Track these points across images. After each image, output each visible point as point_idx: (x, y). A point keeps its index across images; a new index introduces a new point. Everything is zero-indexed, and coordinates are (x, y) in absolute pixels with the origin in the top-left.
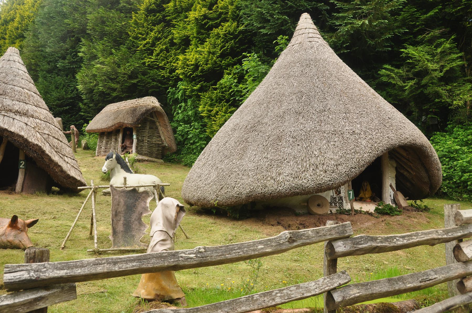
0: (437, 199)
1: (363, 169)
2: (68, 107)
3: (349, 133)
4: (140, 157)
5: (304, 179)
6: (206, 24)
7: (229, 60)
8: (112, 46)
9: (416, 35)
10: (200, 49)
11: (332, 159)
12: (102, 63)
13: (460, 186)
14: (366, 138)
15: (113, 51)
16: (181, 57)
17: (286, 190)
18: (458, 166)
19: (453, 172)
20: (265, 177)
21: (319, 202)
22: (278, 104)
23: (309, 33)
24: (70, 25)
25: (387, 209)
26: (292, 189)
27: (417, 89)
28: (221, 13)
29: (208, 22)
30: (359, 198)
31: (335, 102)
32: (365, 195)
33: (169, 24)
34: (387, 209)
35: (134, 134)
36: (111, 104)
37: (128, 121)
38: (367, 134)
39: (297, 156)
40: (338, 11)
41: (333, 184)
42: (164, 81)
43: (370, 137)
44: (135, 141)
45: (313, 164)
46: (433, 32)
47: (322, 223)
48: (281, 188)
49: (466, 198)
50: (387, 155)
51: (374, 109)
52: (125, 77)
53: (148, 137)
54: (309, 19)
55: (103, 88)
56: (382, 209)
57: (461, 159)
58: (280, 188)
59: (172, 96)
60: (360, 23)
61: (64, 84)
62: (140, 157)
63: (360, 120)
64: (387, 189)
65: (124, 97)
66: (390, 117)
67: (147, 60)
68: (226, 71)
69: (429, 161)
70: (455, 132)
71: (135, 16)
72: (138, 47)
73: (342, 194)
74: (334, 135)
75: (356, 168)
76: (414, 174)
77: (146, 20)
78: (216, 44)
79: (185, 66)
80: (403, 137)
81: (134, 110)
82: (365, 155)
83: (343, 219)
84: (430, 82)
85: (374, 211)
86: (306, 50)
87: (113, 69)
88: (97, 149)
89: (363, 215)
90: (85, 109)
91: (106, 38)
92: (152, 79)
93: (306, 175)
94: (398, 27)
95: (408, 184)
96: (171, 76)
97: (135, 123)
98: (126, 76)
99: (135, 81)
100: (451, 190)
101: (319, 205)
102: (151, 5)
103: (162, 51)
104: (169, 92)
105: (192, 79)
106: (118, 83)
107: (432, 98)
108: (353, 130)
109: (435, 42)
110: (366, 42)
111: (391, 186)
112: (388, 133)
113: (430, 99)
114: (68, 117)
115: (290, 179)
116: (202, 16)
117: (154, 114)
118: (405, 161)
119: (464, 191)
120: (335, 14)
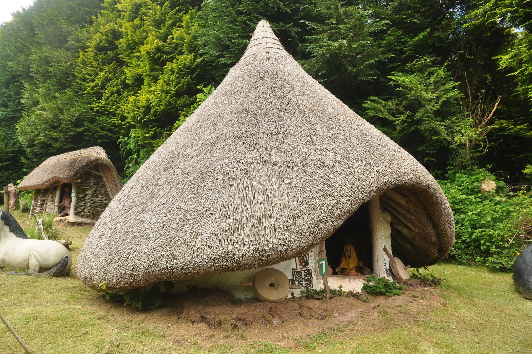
0: (443, 264)
1: (340, 223)
2: (8, 163)
3: (315, 164)
4: (80, 220)
5: (238, 242)
6: (159, 58)
7: (184, 99)
8: (56, 90)
9: (405, 62)
10: (153, 88)
11: (285, 207)
12: (44, 110)
13: (470, 246)
14: (343, 172)
15: (57, 94)
16: (131, 99)
17: (207, 263)
18: (466, 220)
19: (460, 229)
20: (173, 241)
21: (272, 280)
22: (211, 128)
23: (266, 43)
24: (12, 67)
25: (381, 286)
26: (216, 261)
27: (410, 125)
28: (177, 45)
29: (162, 56)
30: (340, 270)
31: (295, 122)
32: (348, 264)
33: (122, 63)
34: (381, 286)
35: (72, 191)
36: (52, 157)
37: (64, 175)
38: (344, 166)
39: (227, 203)
40: (311, 32)
41: (287, 249)
42: (116, 130)
43: (349, 170)
44: (74, 200)
45: (253, 217)
46: (423, 58)
47: (275, 315)
48: (197, 260)
49: (479, 261)
50: (378, 201)
51: (355, 132)
52: (68, 124)
53: (92, 195)
54: (267, 27)
55: (44, 138)
56: (373, 286)
57: (470, 212)
58: (195, 259)
59: (125, 147)
60: (337, 44)
61: (5, 136)
62: (80, 220)
63: (334, 146)
64: (380, 254)
65: (68, 148)
66: (379, 143)
67: (95, 105)
68: (181, 113)
69: (438, 210)
70: (457, 179)
71: (83, 55)
72: (85, 90)
73: (311, 266)
74: (291, 168)
75: (327, 221)
76: (417, 231)
77: (96, 59)
78: (171, 81)
79: (136, 109)
80: (400, 172)
81: (73, 162)
82: (342, 200)
83: (310, 308)
84: (425, 115)
85: (362, 290)
86: (260, 61)
87: (55, 115)
88: (31, 211)
89: (344, 299)
90: (29, 165)
91: (50, 80)
92: (100, 128)
93: (241, 235)
94: (383, 53)
95: (409, 247)
96: (123, 123)
97: (72, 177)
98: (70, 123)
99: (81, 129)
100: (460, 251)
101: (272, 285)
102: (101, 42)
103: (112, 93)
104: (120, 142)
105: (145, 125)
106: (61, 131)
107: (428, 136)
108: (322, 161)
109: (426, 71)
110: (346, 69)
111: (385, 250)
112: (377, 165)
113: (426, 137)
114: (8, 174)
115: (213, 242)
116: (155, 48)
117: (100, 168)
118: (404, 212)
119: (475, 253)
120: (307, 37)
